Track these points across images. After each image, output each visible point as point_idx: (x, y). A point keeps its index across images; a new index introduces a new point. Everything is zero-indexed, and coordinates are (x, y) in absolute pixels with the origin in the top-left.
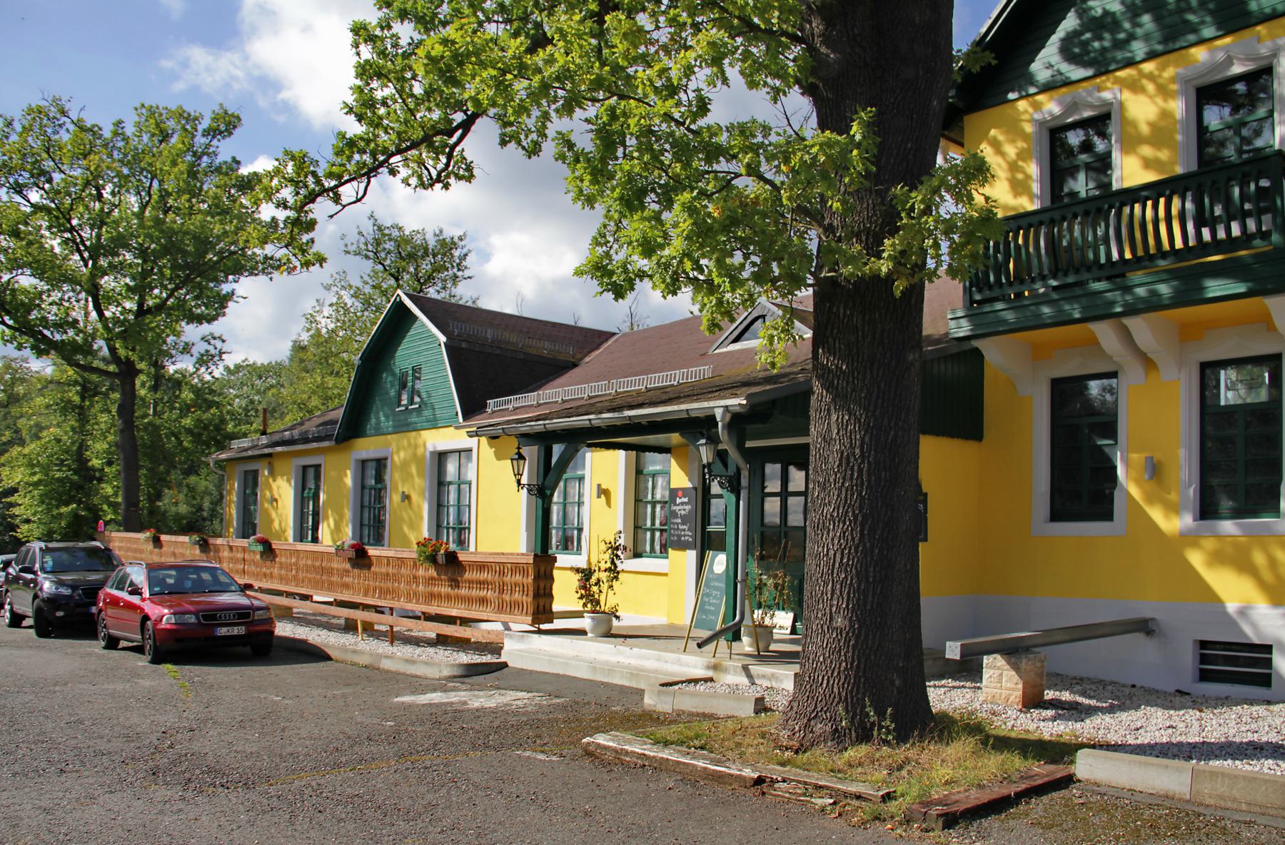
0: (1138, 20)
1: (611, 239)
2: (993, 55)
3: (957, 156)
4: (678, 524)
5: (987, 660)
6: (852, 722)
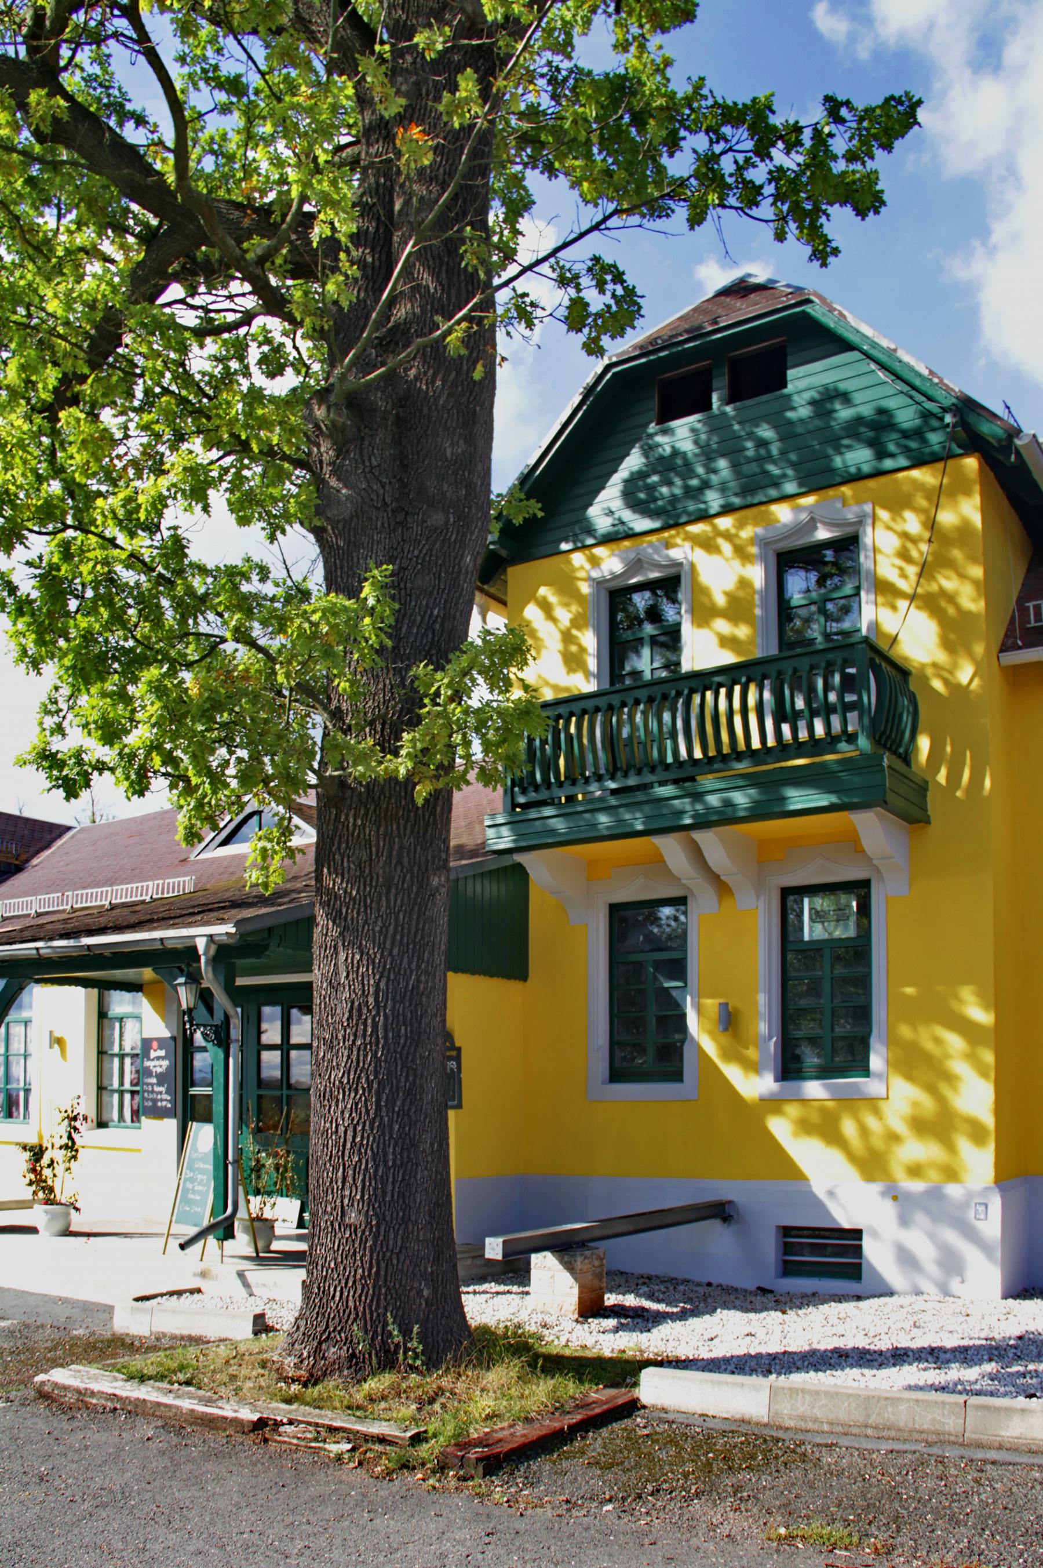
0: (713, 465)
1: (64, 706)
2: (540, 505)
3: (497, 622)
4: (152, 1085)
5: (536, 1259)
6: (372, 1345)
